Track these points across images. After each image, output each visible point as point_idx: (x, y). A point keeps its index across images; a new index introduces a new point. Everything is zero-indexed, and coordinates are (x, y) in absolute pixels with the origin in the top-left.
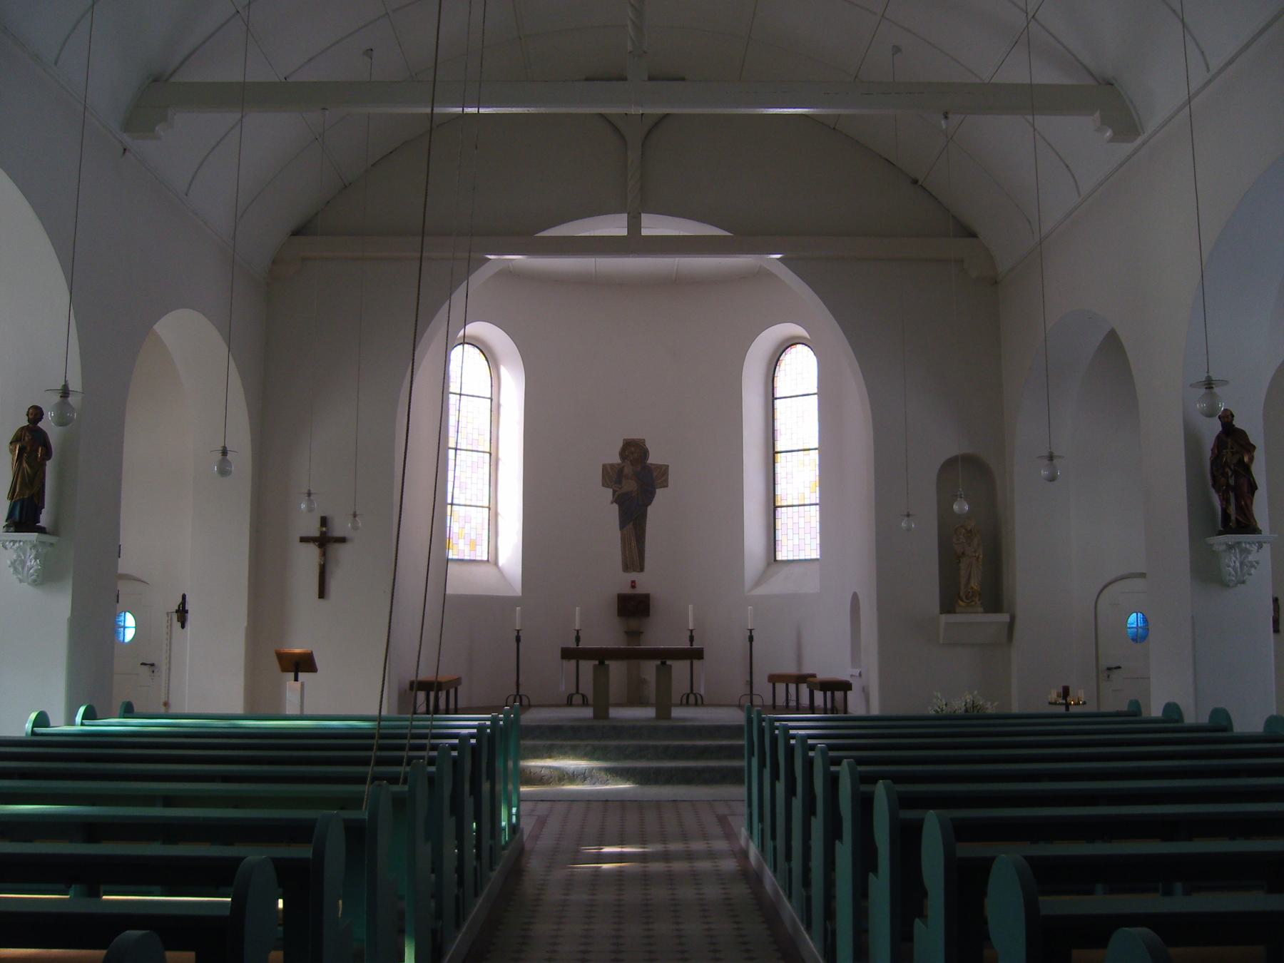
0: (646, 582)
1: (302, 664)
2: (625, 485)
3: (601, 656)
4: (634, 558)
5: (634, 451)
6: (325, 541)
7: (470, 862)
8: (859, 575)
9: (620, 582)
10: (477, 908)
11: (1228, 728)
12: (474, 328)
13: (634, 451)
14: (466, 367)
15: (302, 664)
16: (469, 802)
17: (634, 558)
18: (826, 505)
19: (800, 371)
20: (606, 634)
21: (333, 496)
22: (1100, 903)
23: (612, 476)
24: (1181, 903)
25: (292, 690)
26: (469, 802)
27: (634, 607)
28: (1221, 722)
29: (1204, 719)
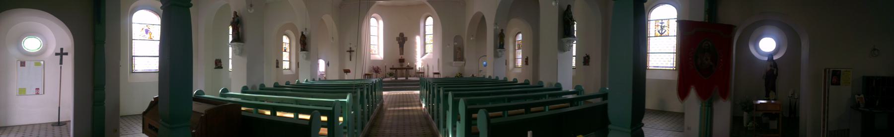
0: (404, 57)
1: (347, 71)
2: (400, 42)
3: (396, 69)
4: (402, 53)
5: (402, 35)
6: (351, 51)
7: (366, 113)
8: (439, 56)
9: (400, 57)
10: (376, 111)
11: (560, 89)
12: (374, 15)
13: (402, 35)
14: (373, 21)
15: (347, 71)
16: (366, 100)
17: (402, 53)
18: (434, 44)
19: (430, 21)
20: (397, 65)
21: (353, 46)
22: (477, 106)
23: (398, 39)
24: (490, 105)
25: (347, 77)
26: (366, 100)
27: (402, 61)
28: (506, 78)
29: (523, 82)
